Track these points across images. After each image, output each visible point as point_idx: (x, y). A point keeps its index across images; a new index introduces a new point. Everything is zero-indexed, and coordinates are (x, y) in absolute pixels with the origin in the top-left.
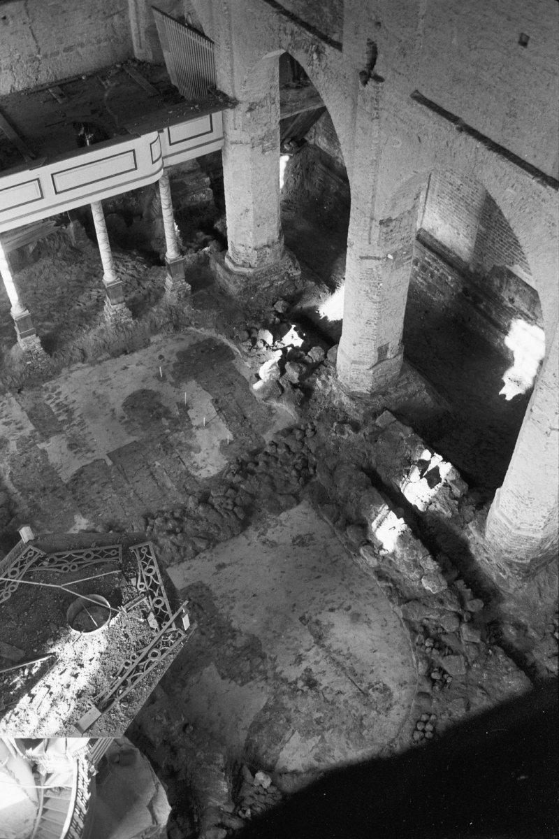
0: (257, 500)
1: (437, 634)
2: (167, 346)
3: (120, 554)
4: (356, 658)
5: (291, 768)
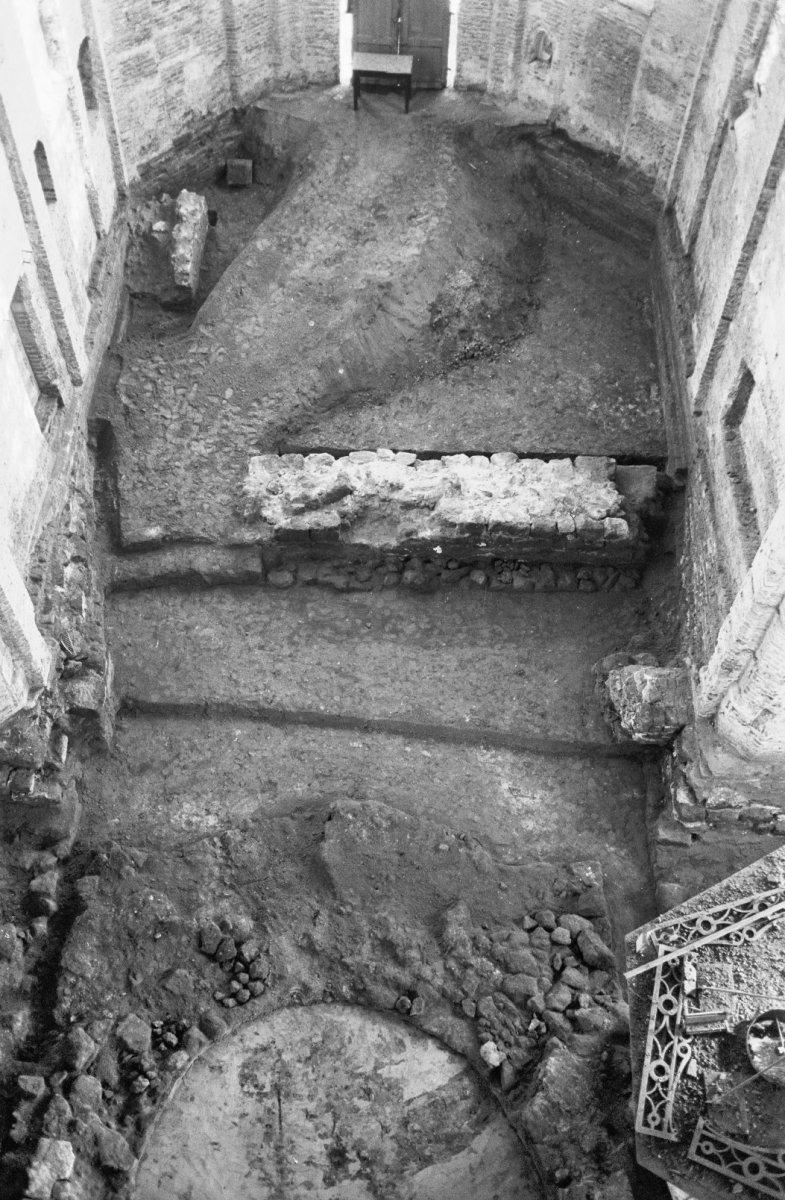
1: (116, 1092)
3: (695, 1142)
4: (248, 1152)
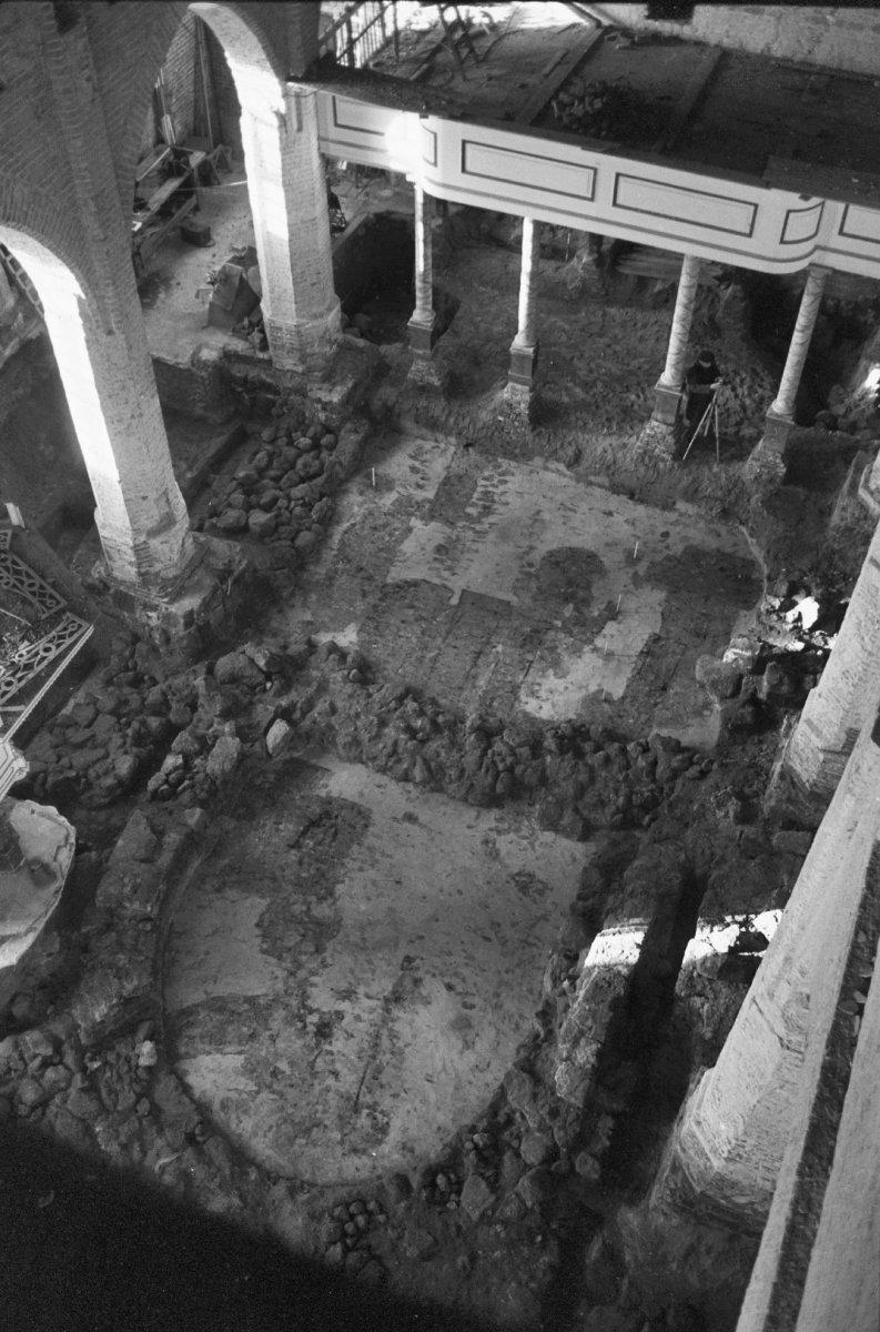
0: (543, 790)
2: (689, 526)
4: (401, 1063)
5: (191, 1080)
